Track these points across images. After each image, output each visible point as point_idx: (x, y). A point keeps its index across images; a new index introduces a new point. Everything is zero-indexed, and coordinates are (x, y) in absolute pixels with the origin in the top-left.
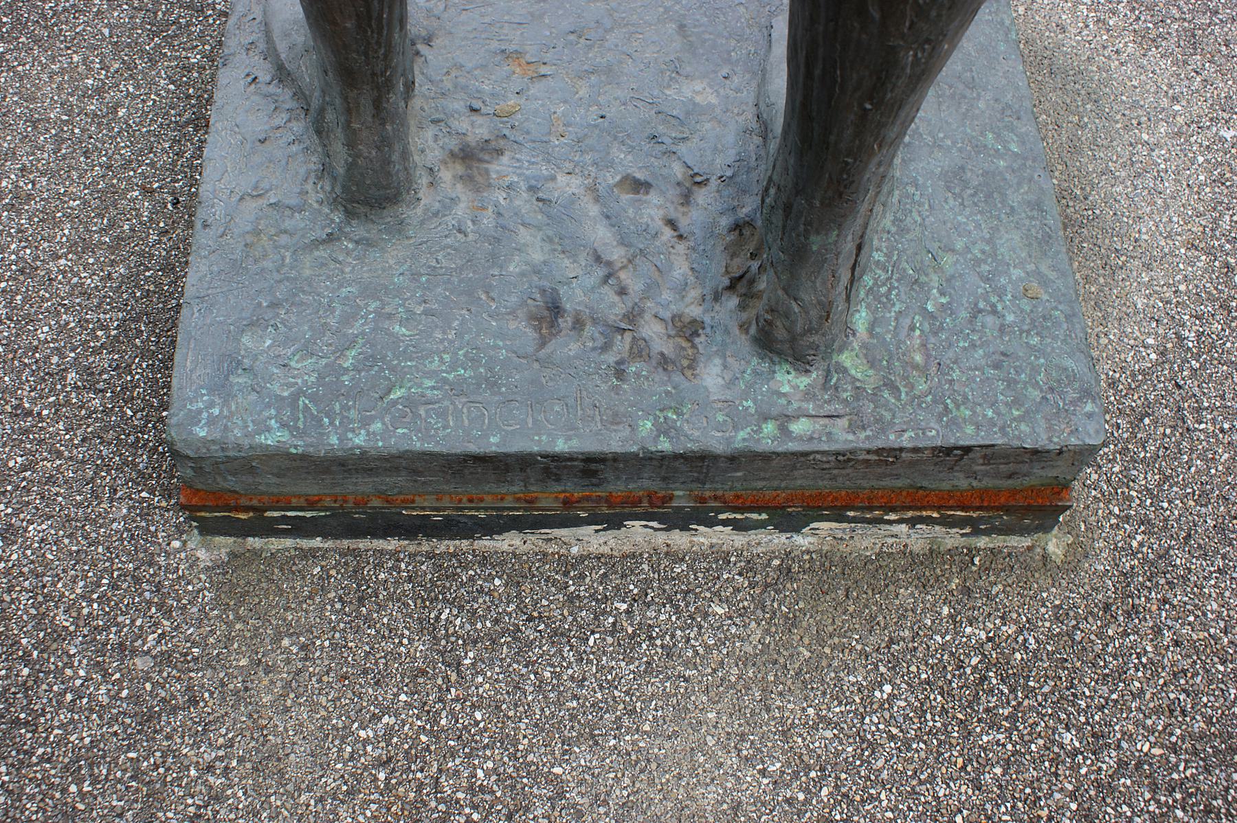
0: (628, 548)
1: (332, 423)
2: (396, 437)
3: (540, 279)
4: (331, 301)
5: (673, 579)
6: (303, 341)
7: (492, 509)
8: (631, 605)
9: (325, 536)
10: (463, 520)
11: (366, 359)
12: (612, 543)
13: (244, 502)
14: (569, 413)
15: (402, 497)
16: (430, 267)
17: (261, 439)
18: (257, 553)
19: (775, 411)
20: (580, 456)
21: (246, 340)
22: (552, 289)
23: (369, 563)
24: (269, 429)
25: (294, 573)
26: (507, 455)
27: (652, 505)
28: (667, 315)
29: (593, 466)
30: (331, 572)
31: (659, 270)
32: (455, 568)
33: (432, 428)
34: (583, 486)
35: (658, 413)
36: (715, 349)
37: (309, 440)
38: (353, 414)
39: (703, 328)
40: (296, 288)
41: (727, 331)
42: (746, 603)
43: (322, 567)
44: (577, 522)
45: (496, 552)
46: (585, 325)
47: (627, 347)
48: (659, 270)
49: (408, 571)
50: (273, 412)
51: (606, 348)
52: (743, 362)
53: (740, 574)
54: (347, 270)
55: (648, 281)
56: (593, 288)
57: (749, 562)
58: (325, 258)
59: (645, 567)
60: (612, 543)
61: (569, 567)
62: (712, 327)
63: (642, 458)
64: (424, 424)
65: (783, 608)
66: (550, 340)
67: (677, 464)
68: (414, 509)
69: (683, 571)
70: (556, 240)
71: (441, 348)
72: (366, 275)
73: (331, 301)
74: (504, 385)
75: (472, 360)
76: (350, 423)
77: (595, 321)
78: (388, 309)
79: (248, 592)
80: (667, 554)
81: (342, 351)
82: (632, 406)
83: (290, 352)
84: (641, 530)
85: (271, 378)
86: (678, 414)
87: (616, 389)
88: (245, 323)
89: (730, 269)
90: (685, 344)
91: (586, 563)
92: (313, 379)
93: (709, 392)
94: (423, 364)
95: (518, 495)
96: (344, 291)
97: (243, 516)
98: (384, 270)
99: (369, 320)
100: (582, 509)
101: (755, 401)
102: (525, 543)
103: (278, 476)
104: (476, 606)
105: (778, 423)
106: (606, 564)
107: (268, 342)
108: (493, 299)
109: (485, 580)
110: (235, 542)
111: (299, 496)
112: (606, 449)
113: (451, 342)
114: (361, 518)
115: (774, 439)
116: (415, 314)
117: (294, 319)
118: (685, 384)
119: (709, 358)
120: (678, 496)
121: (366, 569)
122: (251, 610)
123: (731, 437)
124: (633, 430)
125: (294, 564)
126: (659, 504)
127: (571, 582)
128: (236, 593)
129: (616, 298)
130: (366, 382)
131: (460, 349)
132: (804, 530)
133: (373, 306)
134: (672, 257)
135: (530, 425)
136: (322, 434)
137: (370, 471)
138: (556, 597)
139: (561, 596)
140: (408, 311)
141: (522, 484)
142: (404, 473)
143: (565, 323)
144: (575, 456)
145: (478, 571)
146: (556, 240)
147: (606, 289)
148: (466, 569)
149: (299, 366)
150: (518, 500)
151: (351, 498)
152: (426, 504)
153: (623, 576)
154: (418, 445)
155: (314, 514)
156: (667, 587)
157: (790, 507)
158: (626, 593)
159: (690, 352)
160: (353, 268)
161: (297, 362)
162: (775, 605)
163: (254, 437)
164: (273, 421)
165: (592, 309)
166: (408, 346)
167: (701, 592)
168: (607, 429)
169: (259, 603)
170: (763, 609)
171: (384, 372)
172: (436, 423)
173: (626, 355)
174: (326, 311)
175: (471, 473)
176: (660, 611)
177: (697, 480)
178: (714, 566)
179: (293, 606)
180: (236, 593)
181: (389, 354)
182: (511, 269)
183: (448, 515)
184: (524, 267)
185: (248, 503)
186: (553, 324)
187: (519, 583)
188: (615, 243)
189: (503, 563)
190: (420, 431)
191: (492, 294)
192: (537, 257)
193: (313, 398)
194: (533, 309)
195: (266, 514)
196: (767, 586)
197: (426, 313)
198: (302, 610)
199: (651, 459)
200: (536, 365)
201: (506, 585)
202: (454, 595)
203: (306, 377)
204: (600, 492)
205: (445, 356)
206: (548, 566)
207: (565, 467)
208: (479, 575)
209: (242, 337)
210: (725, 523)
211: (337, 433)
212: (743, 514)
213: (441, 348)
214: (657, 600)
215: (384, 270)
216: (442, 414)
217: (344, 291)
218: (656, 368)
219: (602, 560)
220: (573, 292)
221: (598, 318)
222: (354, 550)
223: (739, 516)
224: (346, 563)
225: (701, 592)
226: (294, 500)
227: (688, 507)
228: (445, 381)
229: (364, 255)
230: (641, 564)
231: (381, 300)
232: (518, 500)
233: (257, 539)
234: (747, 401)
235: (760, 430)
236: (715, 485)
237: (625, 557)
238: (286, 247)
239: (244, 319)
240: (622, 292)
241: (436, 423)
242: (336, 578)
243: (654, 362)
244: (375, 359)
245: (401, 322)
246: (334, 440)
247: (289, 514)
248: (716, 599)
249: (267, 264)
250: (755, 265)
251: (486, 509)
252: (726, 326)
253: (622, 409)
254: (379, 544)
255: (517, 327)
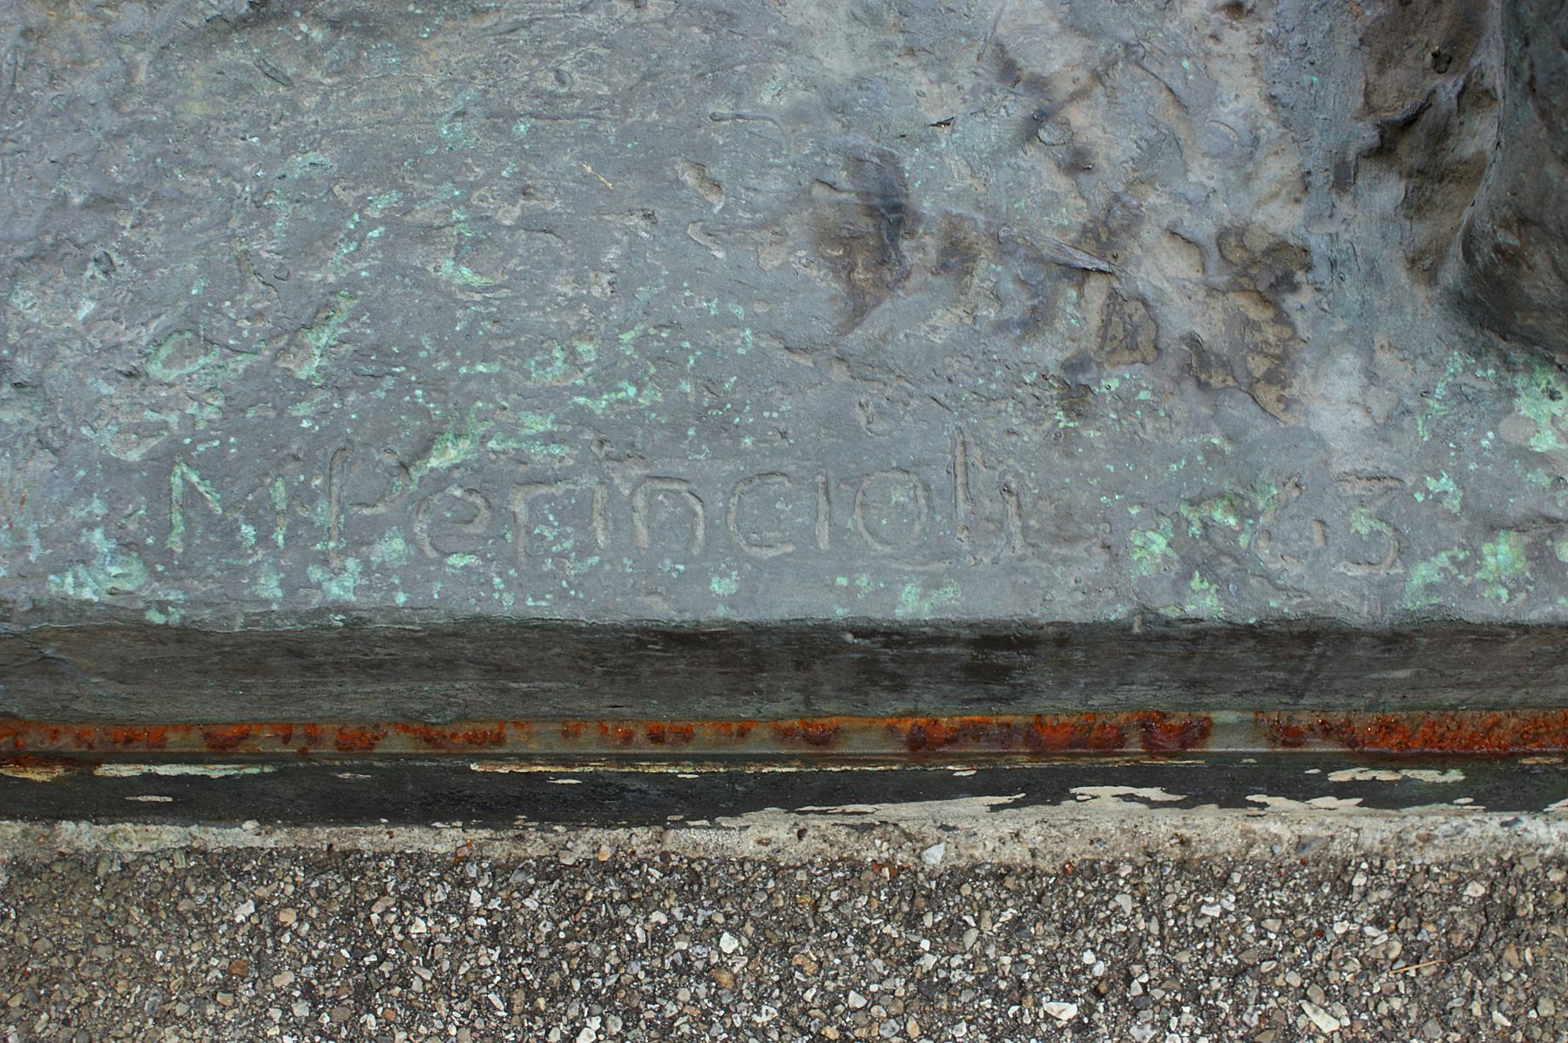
0: (1076, 850)
1: (264, 539)
2: (444, 578)
3: (847, 127)
4: (264, 191)
5: (1201, 935)
6: (183, 304)
7: (715, 758)
8: (1089, 1009)
9: (266, 819)
10: (636, 784)
11: (361, 355)
12: (1033, 835)
13: (34, 741)
14: (931, 508)
15: (468, 728)
16: (538, 93)
17: (69, 586)
18: (82, 864)
19: (1516, 507)
20: (965, 633)
21: (23, 299)
22: (882, 156)
23: (384, 893)
24: (85, 557)
25: (182, 919)
26: (758, 631)
27: (1152, 748)
28: (1205, 229)
29: (1000, 657)
30: (283, 917)
31: (1178, 101)
32: (616, 905)
33: (548, 553)
34: (965, 702)
35: (1184, 510)
36: (1340, 326)
37: (200, 588)
38: (324, 513)
39: (1308, 268)
40: (164, 155)
41: (1374, 276)
42: (1396, 1004)
43: (259, 903)
44: (948, 789)
45: (725, 862)
46: (974, 259)
47: (1095, 320)
48: (1178, 101)
49: (490, 914)
50: (98, 507)
51: (1035, 322)
52: (1421, 365)
53: (1379, 922)
54: (309, 102)
55: (1151, 133)
56: (996, 153)
57: (1402, 889)
58: (247, 70)
59: (1125, 902)
60: (1033, 835)
61: (921, 902)
62: (1333, 264)
63: (1138, 638)
64: (523, 542)
65: (1497, 1016)
66: (879, 302)
67: (1235, 651)
68: (501, 758)
69: (1225, 913)
70: (891, 18)
71: (572, 322)
72: (359, 118)
73: (264, 191)
74: (750, 430)
75: (658, 358)
76: (317, 539)
77: (1003, 248)
78: (421, 214)
79: (60, 970)
80: (1182, 865)
81: (292, 334)
82: (1110, 491)
83: (146, 335)
84: (1113, 805)
85: (92, 411)
86: (1242, 515)
87: (1063, 440)
88: (20, 252)
89: (1376, 100)
90: (1255, 312)
91: (966, 890)
92: (210, 413)
93: (1329, 451)
94: (519, 369)
95: (786, 724)
96: (299, 164)
97: (37, 775)
98: (410, 104)
99: (367, 246)
100: (962, 759)
101: (1461, 479)
102: (801, 834)
103: (121, 679)
104: (671, 1009)
105: (1526, 539)
106: (1018, 893)
107: (87, 308)
108: (717, 185)
109: (696, 939)
110: (25, 833)
111: (188, 727)
112: (1038, 614)
113: (599, 307)
114: (359, 782)
115: (1517, 585)
116: (498, 226)
117: (158, 240)
118: (1260, 428)
119: (1326, 352)
120: (1226, 726)
121: (378, 908)
122: (67, 1022)
123: (1392, 580)
124: (1115, 558)
125: (185, 893)
126: (1173, 746)
127: (925, 945)
128: (26, 976)
129: (1062, 183)
130: (362, 420)
131: (623, 328)
132: (1553, 807)
133: (382, 203)
134: (1215, 65)
135: (823, 545)
136: (238, 571)
137: (376, 669)
138: (887, 985)
139: (900, 982)
140: (479, 218)
141: (798, 697)
142: (470, 673)
143: (919, 251)
144: (952, 631)
145: (677, 912)
146: (891, 18)
147: (1031, 157)
148: (644, 906)
149: (173, 374)
150: (786, 735)
151: (329, 731)
152: (534, 747)
153: (1067, 927)
154: (506, 603)
155: (231, 770)
156: (1184, 958)
157: (1532, 754)
158: (1074, 974)
159: (1271, 334)
160: (325, 96)
161: (167, 364)
162: (1476, 1008)
163: (43, 578)
164: (98, 534)
165: (993, 210)
166: (478, 317)
167: (1275, 973)
168: (1043, 557)
169: (90, 1001)
170: (1444, 1016)
171: (410, 391)
172: (557, 540)
173: (1090, 343)
174: (246, 221)
175: (658, 673)
176: (1165, 1023)
177: (1284, 688)
178: (1308, 900)
179: (180, 1010)
180: (26, 976)
181: (425, 340)
182: (766, 99)
183: (596, 774)
184: (800, 94)
185: (46, 746)
186: (884, 256)
187: (785, 945)
188: (1054, 26)
189: (744, 890)
190: (512, 561)
191: (713, 171)
192: (838, 64)
193: (211, 468)
194: (829, 212)
195: (100, 771)
196: (1452, 955)
197: (528, 224)
198: (204, 1020)
199: (1164, 638)
200: (839, 373)
201: (752, 952)
202: (612, 981)
203: (192, 409)
204: (1013, 716)
205: (583, 347)
206: (863, 900)
207: (921, 659)
208: (680, 925)
209: (12, 291)
210: (1342, 791)
211: (278, 568)
212: (1396, 770)
213: (572, 322)
214: (1157, 994)
215: (410, 104)
216: (576, 513)
217: (299, 164)
218: (1177, 381)
219: (1010, 883)
220: (942, 165)
221: (1011, 239)
222: (346, 854)
223: (1384, 776)
224: (323, 893)
225: (1275, 973)
226: (173, 738)
227: (1251, 755)
228: (583, 418)
229: (355, 61)
230: (1114, 893)
231: (403, 188)
232: (786, 735)
233: (84, 825)
234: (1437, 477)
235: (1474, 560)
236: (1328, 699)
237: (1068, 873)
238: (134, 38)
239: (21, 242)
240: (1078, 164)
241: (557, 540)
242: (295, 933)
243: (1171, 364)
244: (386, 359)
245: (458, 248)
246: (270, 587)
247: (163, 770)
248: (1315, 992)
249: (86, 86)
250: (1447, 88)
251: (697, 759)
252: (1371, 261)
253: (1084, 499)
254: (412, 838)
255: (785, 266)
